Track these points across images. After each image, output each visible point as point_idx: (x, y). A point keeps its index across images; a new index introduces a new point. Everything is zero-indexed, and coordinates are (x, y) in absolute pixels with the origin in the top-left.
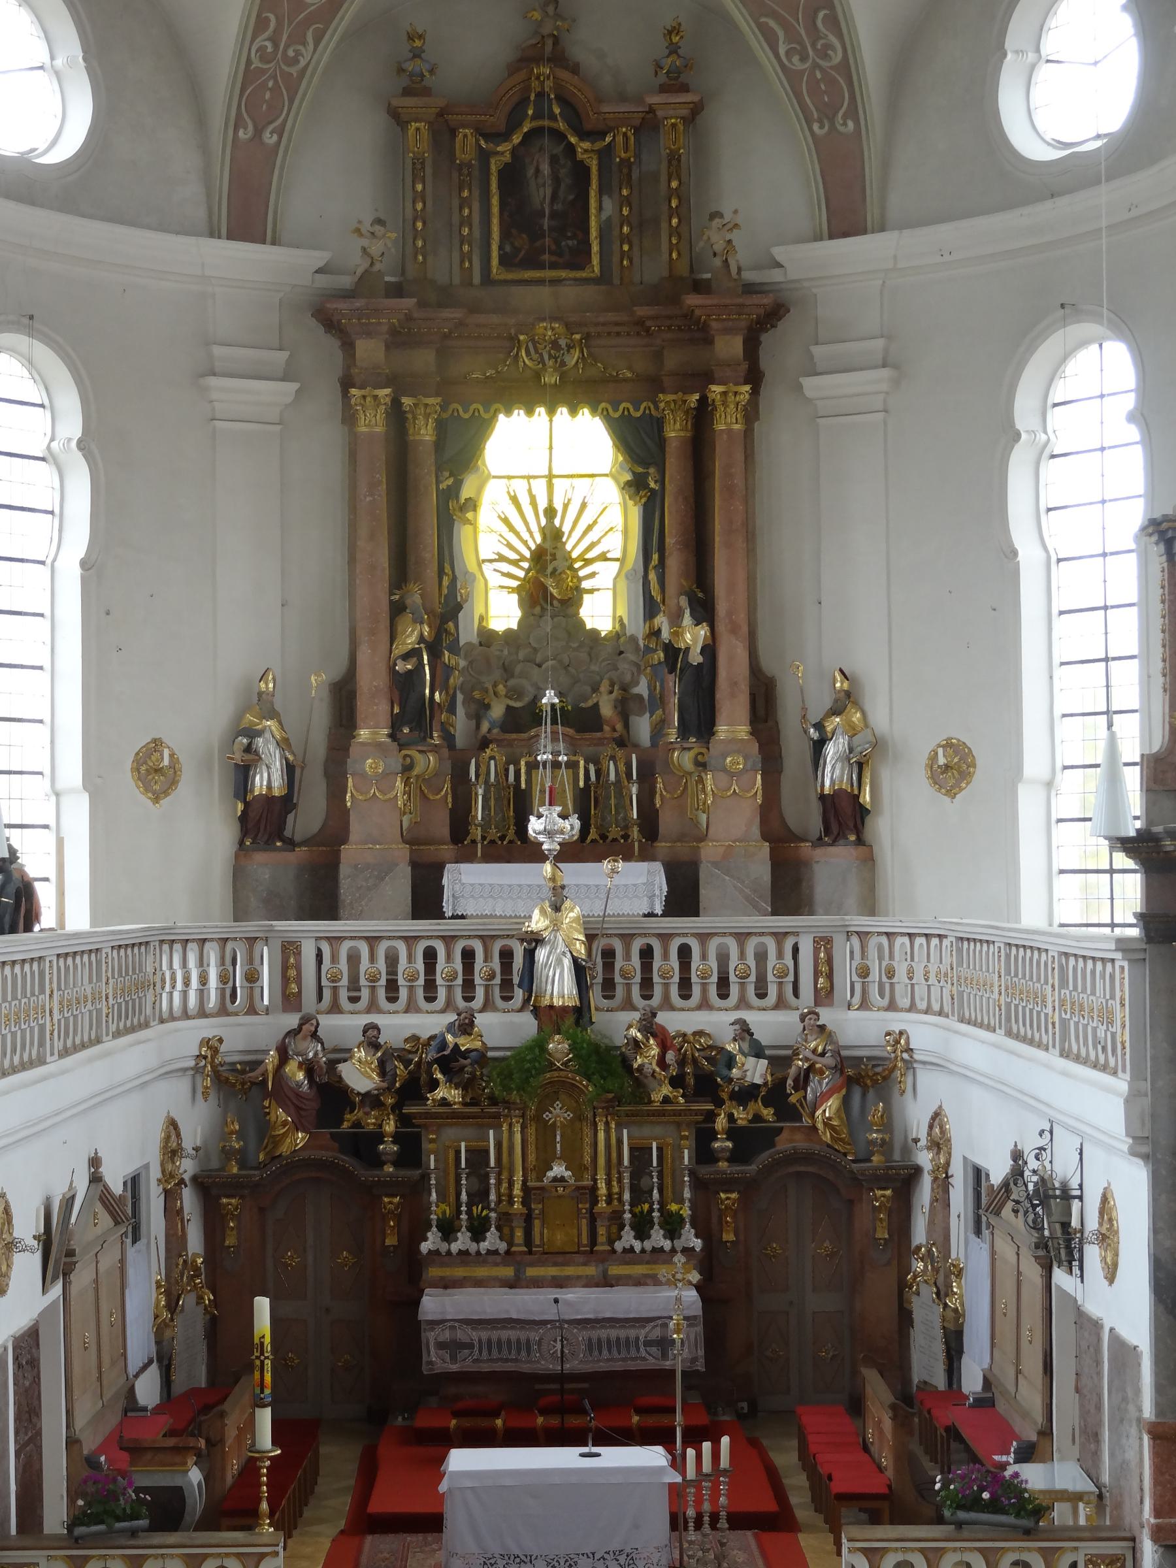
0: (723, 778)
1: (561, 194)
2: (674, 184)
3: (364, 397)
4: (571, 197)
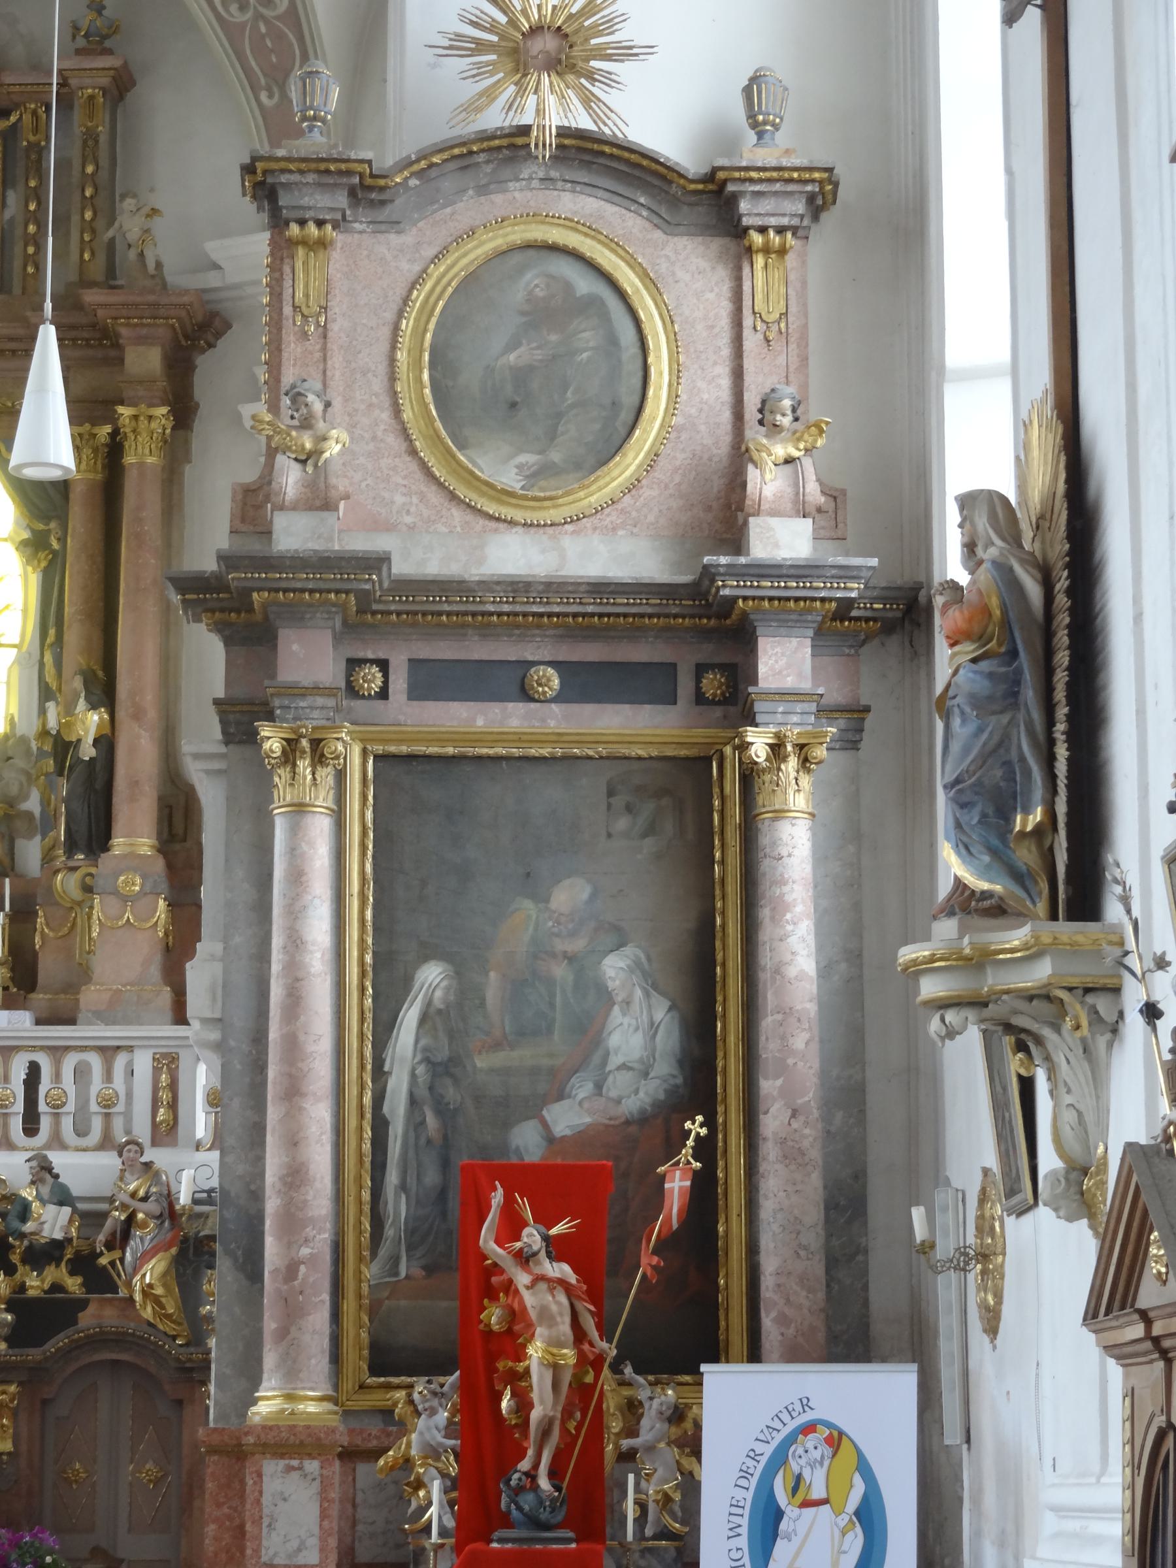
0: (113, 903)
2: (90, 169)
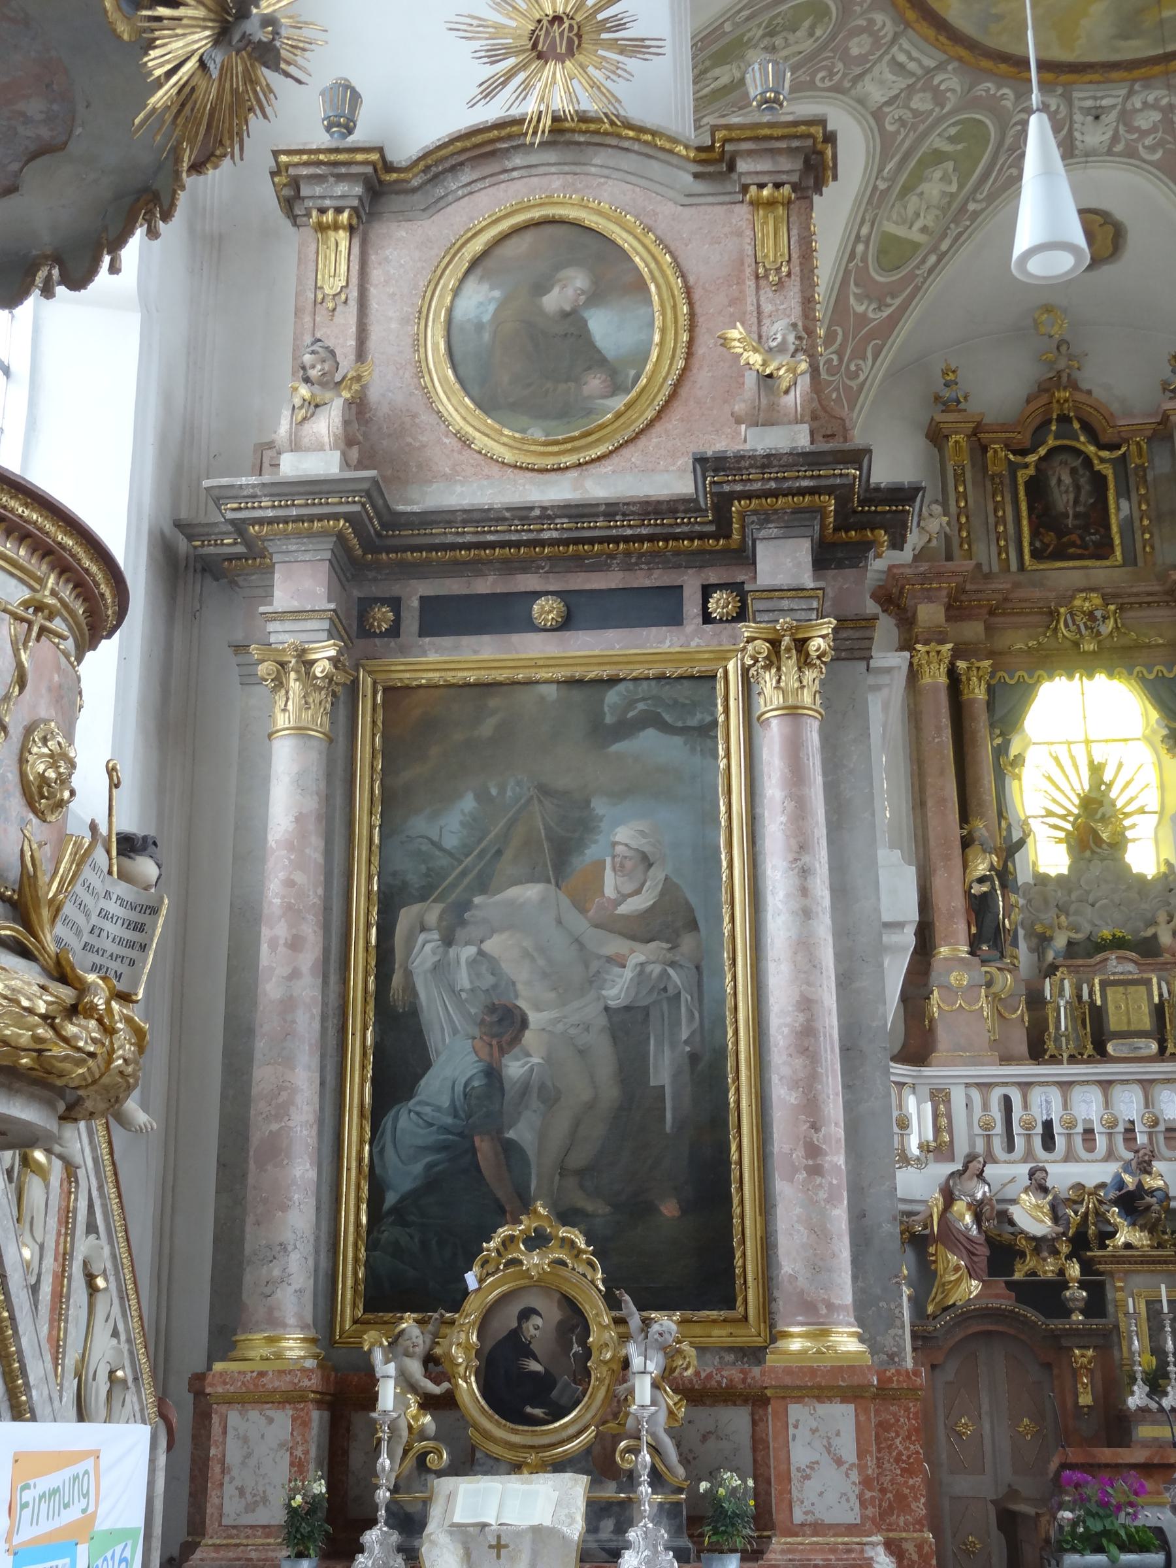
1: (1082, 498)
3: (928, 652)
4: (1092, 501)
